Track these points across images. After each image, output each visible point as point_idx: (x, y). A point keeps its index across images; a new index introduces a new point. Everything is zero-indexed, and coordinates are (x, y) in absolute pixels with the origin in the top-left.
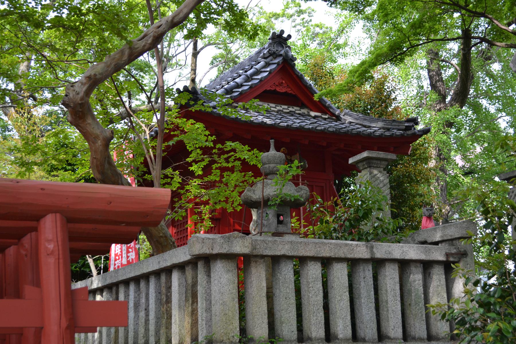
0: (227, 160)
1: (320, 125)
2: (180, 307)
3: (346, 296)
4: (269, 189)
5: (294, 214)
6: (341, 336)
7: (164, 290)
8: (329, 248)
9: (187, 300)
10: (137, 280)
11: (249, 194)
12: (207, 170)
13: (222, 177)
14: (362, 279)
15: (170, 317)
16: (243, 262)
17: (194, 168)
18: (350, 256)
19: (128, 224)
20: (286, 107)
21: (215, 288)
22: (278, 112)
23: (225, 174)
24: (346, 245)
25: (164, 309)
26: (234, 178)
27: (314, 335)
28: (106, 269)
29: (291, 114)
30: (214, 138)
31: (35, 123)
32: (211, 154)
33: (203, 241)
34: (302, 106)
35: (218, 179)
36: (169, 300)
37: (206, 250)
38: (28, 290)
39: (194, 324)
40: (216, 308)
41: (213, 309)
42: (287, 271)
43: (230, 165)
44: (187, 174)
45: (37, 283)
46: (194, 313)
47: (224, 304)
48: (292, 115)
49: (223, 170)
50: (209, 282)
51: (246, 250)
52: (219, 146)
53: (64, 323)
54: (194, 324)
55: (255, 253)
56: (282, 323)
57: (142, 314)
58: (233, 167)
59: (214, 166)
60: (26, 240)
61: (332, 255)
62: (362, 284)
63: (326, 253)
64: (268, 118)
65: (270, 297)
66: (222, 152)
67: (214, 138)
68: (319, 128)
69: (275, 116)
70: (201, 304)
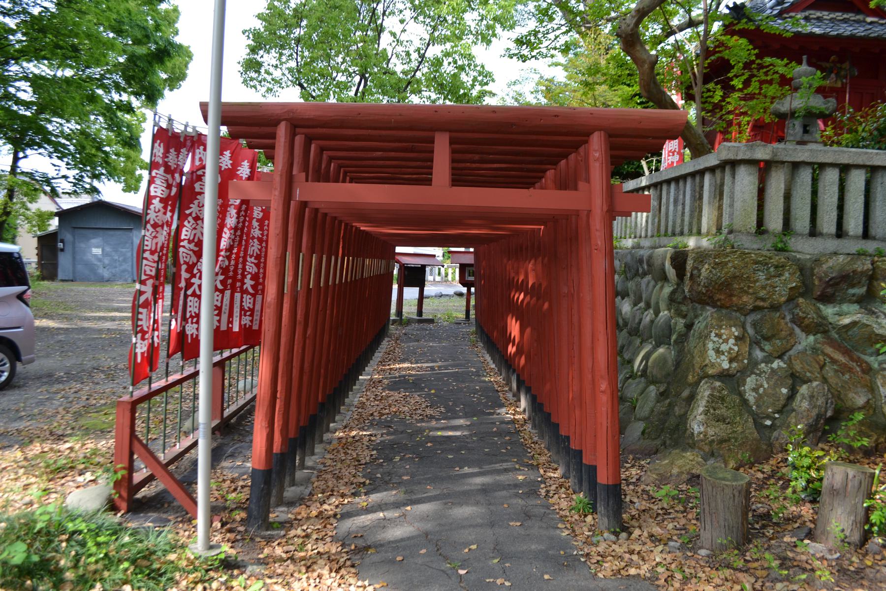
0: (766, 74)
1: (875, 32)
2: (709, 203)
3: (861, 199)
4: (797, 102)
5: (830, 123)
6: (851, 233)
7: (697, 189)
8: (848, 155)
9: (715, 198)
10: (677, 180)
11: (778, 106)
12: (747, 83)
13: (761, 89)
14: (879, 185)
15: (701, 211)
16: (764, 169)
17: (735, 82)
18: (868, 163)
19: (654, 138)
20: (840, 14)
21: (738, 188)
22: (831, 20)
23: (764, 86)
24: (866, 153)
25: (697, 205)
26: (772, 90)
27: (825, 231)
28: (657, 169)
29: (845, 21)
30: (756, 51)
31: (600, 43)
32: (750, 69)
33: (734, 147)
34: (858, 11)
35: (757, 92)
36: (701, 198)
37: (731, 156)
38: (581, 185)
39: (720, 216)
40: (738, 205)
41: (735, 205)
42: (805, 176)
43: (769, 78)
44: (728, 89)
45: (588, 180)
46: (720, 208)
47: (744, 201)
48: (846, 23)
49: (762, 83)
50: (733, 183)
51: (767, 157)
52: (758, 61)
53: (605, 208)
54: (720, 216)
55: (776, 159)
56: (796, 219)
57: (680, 208)
58: (772, 80)
59: (753, 80)
60: (581, 150)
61: (851, 162)
62: (879, 189)
63: (844, 160)
64: (819, 27)
65: (788, 197)
66: (761, 67)
67: (756, 51)
68: (872, 35)
69: (827, 24)
70: (726, 200)
